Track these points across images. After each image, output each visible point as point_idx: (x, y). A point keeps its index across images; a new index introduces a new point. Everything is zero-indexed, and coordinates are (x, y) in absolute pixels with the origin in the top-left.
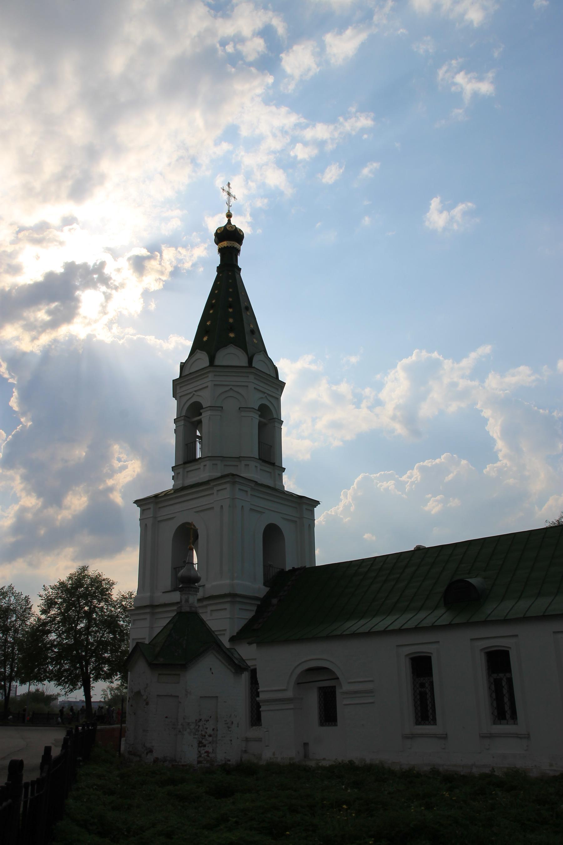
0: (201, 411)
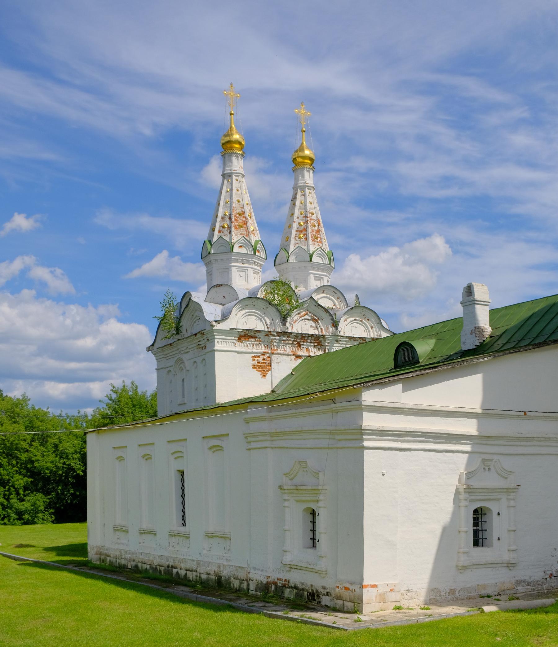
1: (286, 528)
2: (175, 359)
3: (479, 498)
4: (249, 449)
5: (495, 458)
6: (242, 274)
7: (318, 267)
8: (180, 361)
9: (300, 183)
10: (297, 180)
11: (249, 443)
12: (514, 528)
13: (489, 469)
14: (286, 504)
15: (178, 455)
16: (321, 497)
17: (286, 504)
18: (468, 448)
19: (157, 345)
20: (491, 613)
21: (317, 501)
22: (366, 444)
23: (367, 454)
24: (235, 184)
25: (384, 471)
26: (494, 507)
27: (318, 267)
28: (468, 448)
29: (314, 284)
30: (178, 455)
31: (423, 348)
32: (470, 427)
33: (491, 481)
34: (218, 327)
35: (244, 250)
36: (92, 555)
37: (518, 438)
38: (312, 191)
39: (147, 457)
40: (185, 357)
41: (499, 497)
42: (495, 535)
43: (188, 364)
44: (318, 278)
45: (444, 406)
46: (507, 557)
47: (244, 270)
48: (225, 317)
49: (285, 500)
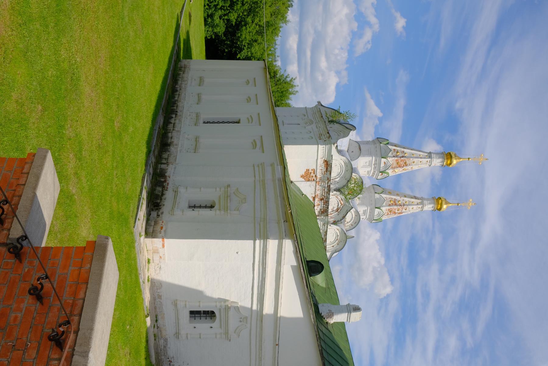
1: (202, 189)
2: (313, 119)
3: (222, 314)
4: (254, 166)
5: (248, 325)
6: (368, 164)
7: (372, 212)
8: (311, 123)
9: (425, 202)
10: (427, 200)
11: (258, 166)
12: (202, 337)
13: (241, 321)
14: (218, 189)
15: (250, 120)
16: (222, 212)
17: (218, 189)
18: (255, 307)
19: (321, 108)
20: (145, 322)
21: (220, 210)
22: (258, 242)
23: (250, 243)
24: (424, 160)
25: (239, 253)
26: (216, 324)
27: (372, 212)
28: (255, 307)
29: (361, 210)
30: (250, 120)
31: (319, 279)
32: (268, 309)
33: (233, 323)
34: (334, 148)
35: (382, 165)
36: (185, 62)
37: (261, 340)
38: (420, 209)
39: (249, 100)
40: (314, 126)
41: (222, 327)
42: (197, 325)
43: (309, 128)
44: (365, 212)
45: (282, 292)
46: (183, 332)
47: (370, 165)
48: (340, 152)
49: (220, 189)
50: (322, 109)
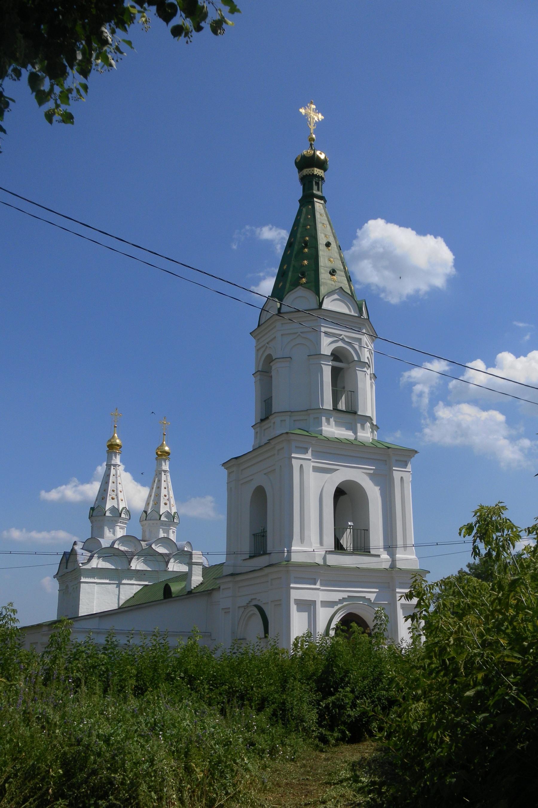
0: (271, 364)
50: (60, 574)
